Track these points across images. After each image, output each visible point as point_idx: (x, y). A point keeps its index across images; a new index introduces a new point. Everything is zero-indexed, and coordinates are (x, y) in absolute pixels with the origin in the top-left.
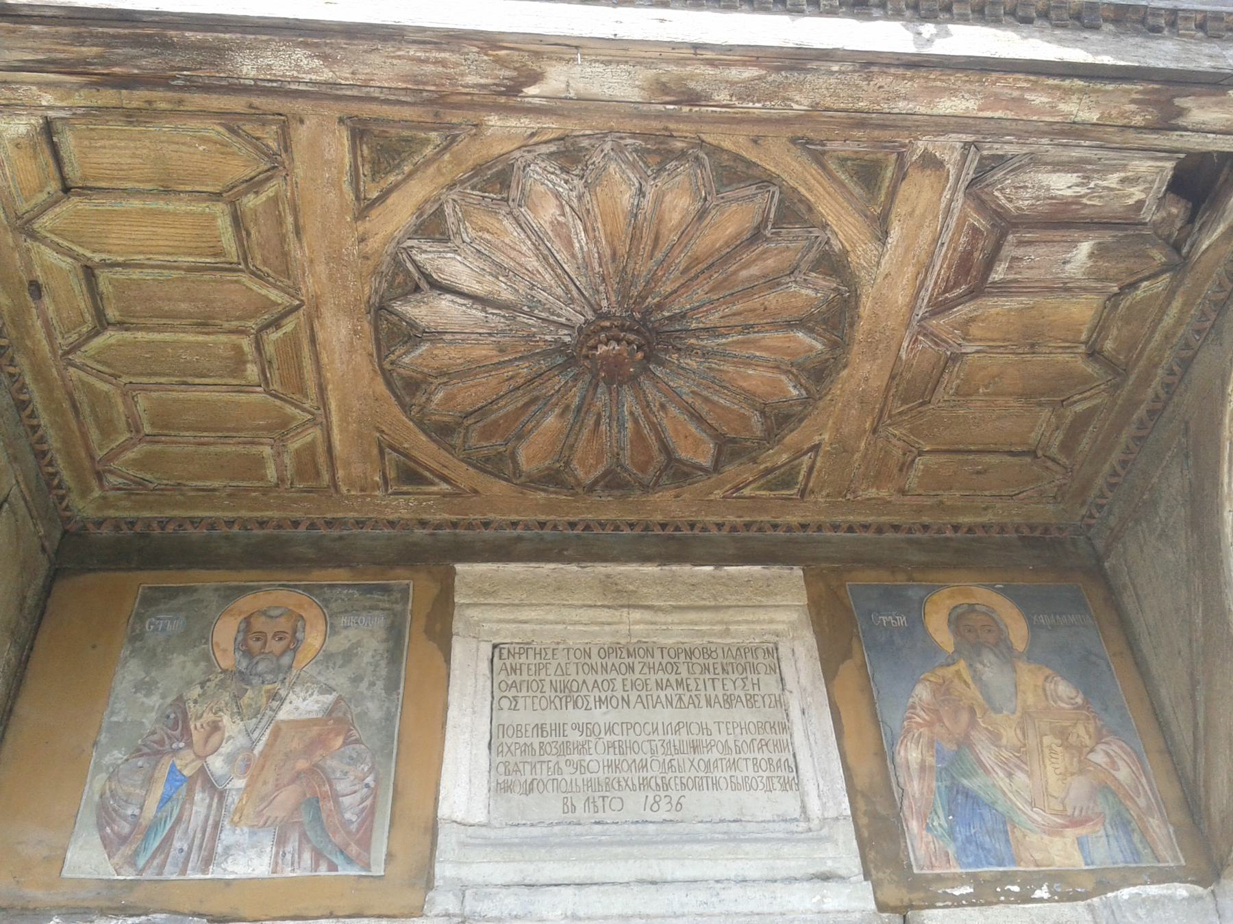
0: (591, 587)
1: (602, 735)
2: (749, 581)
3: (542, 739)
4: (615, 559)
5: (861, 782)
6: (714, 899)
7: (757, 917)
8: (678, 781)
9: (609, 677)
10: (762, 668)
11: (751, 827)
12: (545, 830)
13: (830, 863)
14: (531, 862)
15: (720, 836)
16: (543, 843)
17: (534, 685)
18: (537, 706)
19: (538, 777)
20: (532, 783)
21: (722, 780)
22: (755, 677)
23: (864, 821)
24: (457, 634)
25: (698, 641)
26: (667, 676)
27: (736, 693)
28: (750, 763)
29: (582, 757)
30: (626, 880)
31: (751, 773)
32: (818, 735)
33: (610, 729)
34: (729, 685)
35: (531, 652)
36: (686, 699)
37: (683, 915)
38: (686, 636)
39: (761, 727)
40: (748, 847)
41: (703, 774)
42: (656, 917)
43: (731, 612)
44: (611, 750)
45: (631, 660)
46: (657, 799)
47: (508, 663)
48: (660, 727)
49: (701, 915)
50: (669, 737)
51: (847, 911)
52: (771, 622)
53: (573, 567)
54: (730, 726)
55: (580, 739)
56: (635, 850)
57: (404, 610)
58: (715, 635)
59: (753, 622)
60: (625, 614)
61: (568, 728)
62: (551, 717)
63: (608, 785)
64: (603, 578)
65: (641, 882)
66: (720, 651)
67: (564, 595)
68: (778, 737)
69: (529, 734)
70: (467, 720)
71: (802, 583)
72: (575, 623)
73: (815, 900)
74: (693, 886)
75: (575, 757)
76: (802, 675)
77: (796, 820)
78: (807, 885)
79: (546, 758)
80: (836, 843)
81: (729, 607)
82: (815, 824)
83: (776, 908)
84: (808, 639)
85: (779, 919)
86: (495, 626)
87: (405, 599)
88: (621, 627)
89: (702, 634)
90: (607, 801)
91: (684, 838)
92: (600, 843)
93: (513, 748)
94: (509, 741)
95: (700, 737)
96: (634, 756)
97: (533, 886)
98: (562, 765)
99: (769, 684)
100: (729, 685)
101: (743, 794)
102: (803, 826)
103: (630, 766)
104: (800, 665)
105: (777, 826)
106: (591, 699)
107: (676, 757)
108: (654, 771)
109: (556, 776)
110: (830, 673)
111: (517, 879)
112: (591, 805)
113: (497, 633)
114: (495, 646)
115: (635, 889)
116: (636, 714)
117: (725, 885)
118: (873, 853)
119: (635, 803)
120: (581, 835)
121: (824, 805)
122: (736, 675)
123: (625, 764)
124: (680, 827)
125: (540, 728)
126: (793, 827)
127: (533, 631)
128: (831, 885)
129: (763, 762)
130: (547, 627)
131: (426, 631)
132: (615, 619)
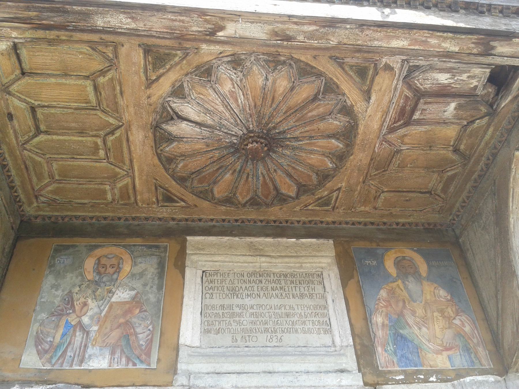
2: (311, 245)
5: (357, 331)
6: (295, 380)
8: (280, 330)
9: (251, 285)
10: (316, 282)
12: (224, 350)
14: (218, 363)
15: (298, 353)
16: (223, 355)
17: (220, 288)
18: (221, 297)
22: (313, 286)
26: (276, 285)
27: (305, 293)
28: (311, 322)
29: (240, 319)
31: (311, 326)
32: (339, 311)
34: (302, 289)
35: (219, 274)
37: (282, 387)
38: (284, 268)
39: (316, 307)
40: (309, 358)
43: (303, 258)
44: (252, 316)
45: (261, 278)
46: (272, 337)
47: (209, 278)
50: (277, 311)
52: (320, 263)
53: (237, 239)
54: (302, 306)
55: (239, 311)
56: (262, 359)
57: (165, 256)
59: (312, 263)
62: (227, 302)
65: (265, 372)
66: (298, 275)
67: (233, 250)
68: (322, 311)
71: (333, 246)
73: (338, 381)
74: (287, 374)
75: (237, 319)
77: (330, 346)
78: (334, 374)
79: (225, 319)
82: (338, 348)
83: (321, 384)
86: (204, 263)
88: (257, 264)
89: (291, 268)
92: (248, 356)
93: (211, 315)
94: (209, 312)
98: (232, 322)
99: (319, 289)
100: (302, 289)
101: (308, 335)
103: (260, 323)
104: (332, 281)
105: (322, 349)
106: (244, 295)
108: (270, 326)
109: (229, 327)
110: (344, 285)
112: (244, 339)
113: (204, 266)
114: (203, 272)
115: (262, 375)
116: (263, 301)
119: (262, 338)
121: (342, 340)
122: (305, 285)
123: (258, 322)
124: (281, 349)
125: (222, 307)
126: (328, 349)
128: (344, 374)
130: (226, 263)
131: (174, 265)
132: (254, 261)
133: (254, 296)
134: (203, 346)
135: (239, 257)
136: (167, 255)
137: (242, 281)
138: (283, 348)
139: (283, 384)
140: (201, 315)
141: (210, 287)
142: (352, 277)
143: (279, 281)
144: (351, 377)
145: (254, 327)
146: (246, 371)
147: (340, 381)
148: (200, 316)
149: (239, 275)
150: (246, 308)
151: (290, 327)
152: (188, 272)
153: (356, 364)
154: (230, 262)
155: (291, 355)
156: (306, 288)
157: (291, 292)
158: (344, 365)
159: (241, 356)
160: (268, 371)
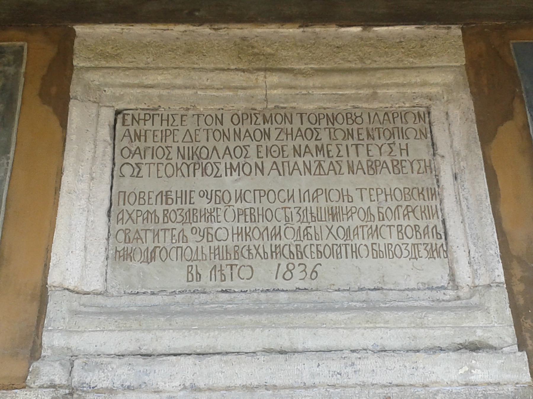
0: (224, 51)
2: (400, 42)
3: (167, 207)
4: (253, 20)
5: (518, 247)
6: (349, 370)
7: (396, 389)
8: (314, 249)
9: (241, 144)
10: (411, 133)
11: (392, 295)
12: (167, 299)
13: (479, 332)
14: (149, 330)
15: (358, 305)
16: (164, 312)
17: (160, 152)
18: (162, 173)
19: (161, 245)
21: (363, 248)
22: (404, 142)
26: (306, 142)
27: (382, 159)
28: (394, 230)
29: (209, 225)
31: (394, 241)
32: (471, 200)
34: (374, 151)
35: (157, 119)
36: (326, 165)
37: (314, 386)
38: (329, 101)
39: (407, 193)
40: (388, 316)
41: (342, 242)
43: (379, 74)
44: (242, 218)
45: (267, 126)
46: (291, 267)
47: (132, 129)
48: (296, 194)
49: (334, 386)
50: (306, 204)
51: (498, 384)
52: (424, 84)
53: (205, 30)
54: (373, 193)
55: (208, 207)
56: (264, 319)
57: (17, 73)
59: (404, 85)
61: (195, 195)
62: (177, 184)
63: (237, 252)
64: (238, 41)
65: (269, 351)
66: (365, 117)
67: (195, 58)
68: (426, 203)
69: (153, 201)
71: (461, 42)
72: (207, 88)
73: (461, 372)
74: (325, 355)
75: (202, 225)
77: (443, 288)
78: (453, 355)
79: (170, 225)
80: (487, 311)
82: (464, 292)
83: (417, 379)
84: (465, 100)
85: (421, 392)
86: (118, 91)
88: (257, 91)
89: (347, 98)
91: (319, 306)
92: (227, 312)
93: (134, 216)
94: (130, 208)
95: (340, 204)
97: (150, 355)
98: (188, 233)
99: (419, 149)
100: (374, 151)
101: (385, 262)
102: (451, 293)
103: (261, 234)
104: (455, 129)
105: (421, 294)
106: (222, 167)
108: (288, 239)
109: (181, 244)
110: (487, 134)
112: (218, 274)
113: (120, 98)
114: (118, 113)
115: (262, 358)
116: (270, 181)
117: (362, 354)
118: (529, 321)
119: (266, 271)
121: (475, 272)
122: (383, 141)
123: (256, 232)
124: (313, 296)
125: (165, 196)
126: (439, 295)
128: (481, 355)
129: (409, 229)
130: (178, 92)
131: (40, 95)
132: (251, 84)
133: (247, 169)
134: (110, 290)
135: (211, 75)
136: (23, 70)
137: (217, 134)
138: (319, 293)
139: (317, 381)
140: (109, 216)
141: (133, 149)
142: (508, 116)
143: (315, 133)
144: (497, 361)
145: (245, 243)
146: (219, 349)
147: (469, 372)
148: (106, 219)
149: (209, 120)
150: (226, 198)
151: (340, 242)
152: (76, 113)
153: (512, 329)
154: (186, 88)
155: (338, 310)
156: (386, 148)
157: (345, 159)
158: (479, 332)
159: (211, 313)
160: (278, 349)
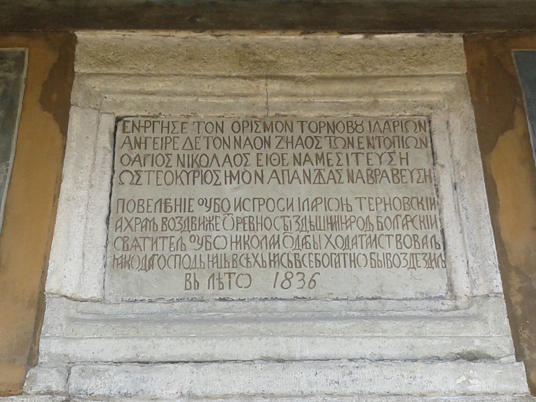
0: (226, 57)
1: (232, 210)
2: (402, 50)
3: (165, 215)
5: (516, 257)
6: (347, 378)
8: (312, 258)
10: (411, 142)
11: (390, 305)
12: (165, 307)
13: (477, 342)
14: (146, 338)
15: (356, 314)
16: (162, 319)
17: (160, 160)
18: (161, 181)
20: (152, 258)
21: (361, 257)
22: (404, 151)
23: (517, 298)
24: (76, 105)
25: (342, 115)
26: (306, 150)
28: (393, 240)
29: (208, 233)
30: (250, 357)
31: (393, 250)
32: (470, 210)
33: (241, 205)
34: (375, 160)
35: (158, 126)
36: (325, 174)
37: (312, 395)
38: (330, 109)
40: (386, 325)
42: (282, 396)
43: (380, 82)
44: (241, 226)
45: (267, 134)
46: (289, 276)
47: (132, 136)
48: (296, 203)
49: (331, 395)
50: (306, 213)
52: (425, 93)
53: (207, 36)
54: (373, 202)
56: (261, 327)
57: (18, 79)
58: (361, 108)
59: (405, 94)
60: (262, 86)
62: (177, 192)
63: (235, 261)
65: (266, 360)
67: (196, 65)
68: (425, 213)
69: (151, 209)
70: (83, 193)
71: (462, 51)
72: (208, 95)
73: (458, 381)
75: (201, 233)
76: (456, 148)
77: (441, 297)
78: (451, 365)
79: (169, 233)
80: (485, 321)
81: (377, 78)
82: (462, 302)
83: (414, 389)
84: (467, 109)
86: (119, 98)
87: (19, 66)
88: (258, 99)
89: (348, 106)
90: (234, 278)
92: (224, 320)
93: (133, 223)
94: (129, 216)
96: (265, 232)
97: (147, 363)
98: (186, 241)
99: (419, 159)
100: (375, 160)
101: (383, 271)
102: (449, 303)
103: (260, 243)
104: (454, 138)
105: (419, 304)
106: (222, 175)
107: (311, 233)
108: (287, 248)
110: (487, 145)
111: (130, 355)
112: (216, 282)
113: (121, 105)
114: (118, 120)
115: (259, 366)
116: (270, 190)
118: (527, 332)
119: (264, 280)
120: (204, 311)
121: (473, 282)
124: (312, 305)
126: (438, 305)
127: (161, 103)
129: (407, 239)
131: (41, 101)
132: (252, 91)
